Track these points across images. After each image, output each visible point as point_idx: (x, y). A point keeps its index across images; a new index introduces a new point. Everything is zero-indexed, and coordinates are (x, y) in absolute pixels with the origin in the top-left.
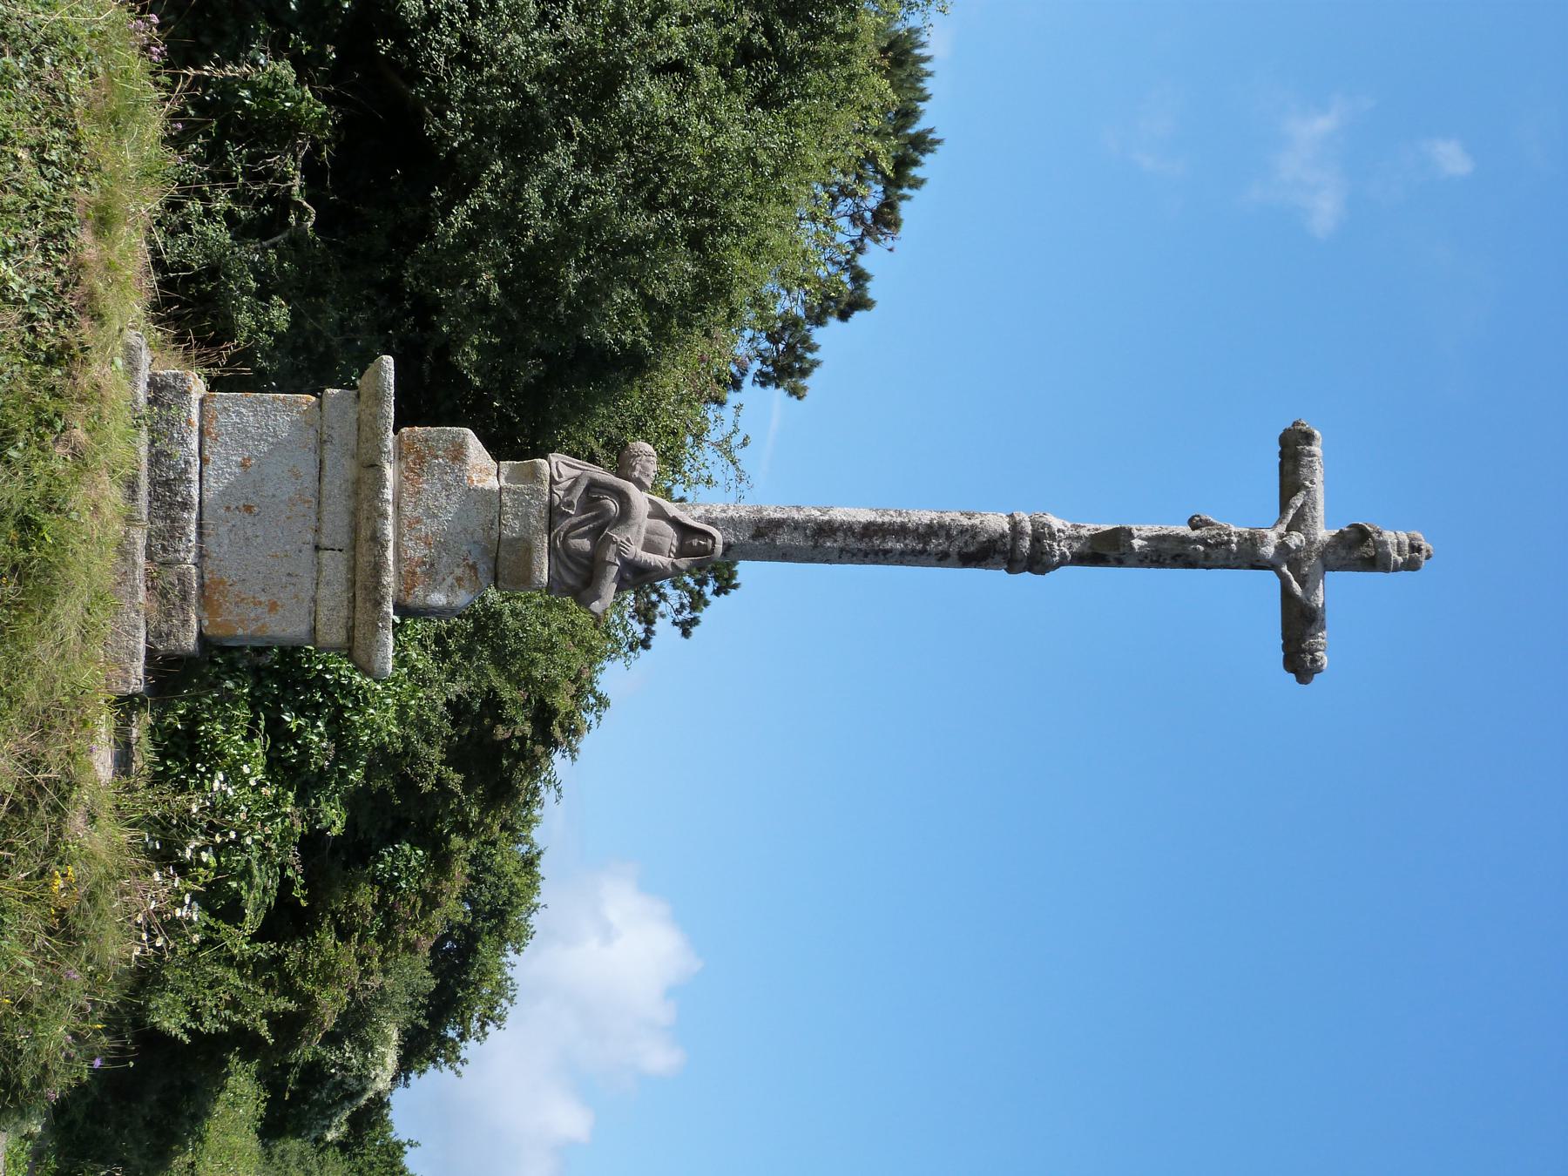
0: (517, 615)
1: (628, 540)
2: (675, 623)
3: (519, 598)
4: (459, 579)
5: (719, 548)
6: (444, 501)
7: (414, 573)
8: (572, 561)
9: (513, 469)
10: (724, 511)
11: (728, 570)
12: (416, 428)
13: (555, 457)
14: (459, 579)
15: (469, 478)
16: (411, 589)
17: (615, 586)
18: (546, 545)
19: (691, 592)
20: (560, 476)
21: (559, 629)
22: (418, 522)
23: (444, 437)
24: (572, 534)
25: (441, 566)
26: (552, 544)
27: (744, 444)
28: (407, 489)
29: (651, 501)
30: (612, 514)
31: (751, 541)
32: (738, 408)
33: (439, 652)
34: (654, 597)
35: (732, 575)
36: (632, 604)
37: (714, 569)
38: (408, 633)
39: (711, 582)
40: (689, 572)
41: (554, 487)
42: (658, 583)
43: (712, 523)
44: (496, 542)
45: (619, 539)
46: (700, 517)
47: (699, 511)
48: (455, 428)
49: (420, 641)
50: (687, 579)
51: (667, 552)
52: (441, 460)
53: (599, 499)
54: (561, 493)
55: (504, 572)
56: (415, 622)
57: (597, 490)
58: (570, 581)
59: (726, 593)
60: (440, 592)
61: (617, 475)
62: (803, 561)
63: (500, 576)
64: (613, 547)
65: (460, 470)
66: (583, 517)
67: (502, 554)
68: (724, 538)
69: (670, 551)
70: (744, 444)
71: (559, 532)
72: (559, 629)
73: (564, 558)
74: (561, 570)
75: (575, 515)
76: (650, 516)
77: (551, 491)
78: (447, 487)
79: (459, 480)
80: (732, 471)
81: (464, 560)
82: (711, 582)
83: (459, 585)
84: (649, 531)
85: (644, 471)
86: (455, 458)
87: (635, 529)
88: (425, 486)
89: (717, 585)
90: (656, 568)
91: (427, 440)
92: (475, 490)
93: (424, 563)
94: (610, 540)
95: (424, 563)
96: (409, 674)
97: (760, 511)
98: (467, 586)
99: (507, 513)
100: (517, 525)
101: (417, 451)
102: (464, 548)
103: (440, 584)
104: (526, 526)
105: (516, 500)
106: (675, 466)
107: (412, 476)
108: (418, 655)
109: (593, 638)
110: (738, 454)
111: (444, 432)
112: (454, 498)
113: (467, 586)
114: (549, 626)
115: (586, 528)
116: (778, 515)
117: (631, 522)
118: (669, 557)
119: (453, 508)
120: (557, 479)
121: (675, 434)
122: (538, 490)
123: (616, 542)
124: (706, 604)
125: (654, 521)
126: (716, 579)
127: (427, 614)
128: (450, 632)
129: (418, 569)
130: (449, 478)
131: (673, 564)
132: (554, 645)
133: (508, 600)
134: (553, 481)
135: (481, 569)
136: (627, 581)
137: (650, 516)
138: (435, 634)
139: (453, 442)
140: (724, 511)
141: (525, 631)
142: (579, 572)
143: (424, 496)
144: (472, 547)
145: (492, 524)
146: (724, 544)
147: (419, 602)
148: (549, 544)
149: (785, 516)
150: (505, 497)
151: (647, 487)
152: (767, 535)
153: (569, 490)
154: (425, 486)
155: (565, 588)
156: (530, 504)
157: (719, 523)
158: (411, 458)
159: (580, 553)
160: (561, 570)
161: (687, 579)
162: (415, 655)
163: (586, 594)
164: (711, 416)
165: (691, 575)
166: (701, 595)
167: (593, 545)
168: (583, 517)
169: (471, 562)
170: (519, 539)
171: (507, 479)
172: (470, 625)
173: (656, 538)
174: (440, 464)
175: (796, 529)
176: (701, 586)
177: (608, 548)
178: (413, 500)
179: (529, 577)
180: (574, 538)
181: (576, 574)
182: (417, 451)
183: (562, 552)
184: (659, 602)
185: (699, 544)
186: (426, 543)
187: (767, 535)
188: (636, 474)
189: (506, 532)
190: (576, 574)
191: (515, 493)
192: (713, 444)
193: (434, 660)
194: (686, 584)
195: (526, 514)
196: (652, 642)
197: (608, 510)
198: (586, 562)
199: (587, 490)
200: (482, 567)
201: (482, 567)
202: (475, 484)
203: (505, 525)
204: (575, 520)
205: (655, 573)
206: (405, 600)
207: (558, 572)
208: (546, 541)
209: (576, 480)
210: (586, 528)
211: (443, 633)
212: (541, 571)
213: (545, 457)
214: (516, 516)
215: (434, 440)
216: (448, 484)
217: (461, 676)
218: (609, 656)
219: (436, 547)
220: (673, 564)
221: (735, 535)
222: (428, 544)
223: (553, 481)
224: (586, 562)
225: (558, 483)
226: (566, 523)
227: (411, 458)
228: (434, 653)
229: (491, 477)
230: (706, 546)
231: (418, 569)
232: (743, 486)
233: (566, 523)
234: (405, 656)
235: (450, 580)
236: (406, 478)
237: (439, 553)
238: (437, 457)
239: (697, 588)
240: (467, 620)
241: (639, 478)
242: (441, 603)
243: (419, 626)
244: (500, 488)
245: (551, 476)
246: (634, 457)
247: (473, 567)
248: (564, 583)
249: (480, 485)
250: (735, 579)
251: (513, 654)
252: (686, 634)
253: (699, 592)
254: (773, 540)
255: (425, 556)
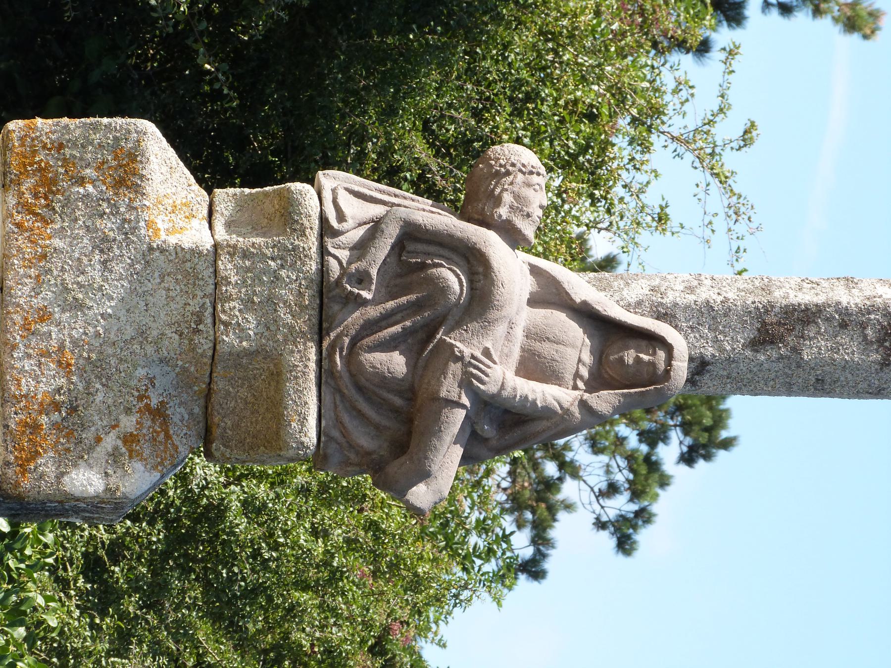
0: (259, 511)
1: (487, 353)
2: (600, 525)
3: (261, 477)
4: (129, 439)
5: (681, 369)
6: (97, 275)
7: (36, 427)
8: (369, 400)
9: (241, 205)
10: (691, 290)
11: (711, 408)
12: (39, 121)
13: (330, 179)
14: (129, 439)
15: (149, 224)
16: (28, 460)
17: (458, 452)
18: (312, 365)
19: (631, 458)
20: (341, 218)
21: (348, 541)
22: (42, 320)
23: (97, 137)
24: (368, 341)
25: (91, 411)
26: (325, 364)
27: (747, 137)
28: (19, 249)
29: (535, 271)
30: (453, 298)
31: (748, 353)
32: (732, 53)
33: (92, 593)
34: (551, 469)
35: (720, 419)
36: (505, 484)
37: (680, 408)
38: (28, 552)
39: (675, 435)
40: (625, 412)
41: (329, 243)
42: (561, 442)
43: (665, 315)
44: (208, 361)
45: (467, 352)
46: (639, 303)
47: (637, 291)
48: (119, 121)
49: (53, 570)
50: (623, 430)
51: (569, 377)
52: (90, 188)
53: (423, 266)
54: (344, 255)
55: (223, 423)
56: (41, 530)
57: (420, 247)
58: (364, 440)
59: (708, 457)
60: (90, 467)
61: (464, 214)
62: (858, 394)
63: (217, 432)
64: (455, 368)
65: (131, 208)
66: (391, 304)
67: (220, 385)
68: (691, 346)
69: (577, 375)
70: (747, 137)
71: (339, 337)
72: (348, 541)
73: (350, 391)
74: (346, 418)
75: (375, 302)
76: (534, 301)
77: (323, 251)
78: (103, 244)
79: (128, 229)
80: (717, 200)
81: (140, 398)
82: (675, 435)
83: (131, 451)
84: (533, 334)
85: (520, 206)
86: (120, 183)
87: (500, 329)
88: (57, 243)
89: (688, 441)
90: (547, 413)
91: (61, 146)
92: (162, 251)
93: (57, 406)
94: (451, 355)
95: (57, 406)
96: (30, 639)
97: (766, 289)
98: (147, 452)
99: (229, 299)
100: (251, 323)
101: (40, 169)
102: (141, 372)
103: (91, 449)
104: (269, 325)
105: (248, 270)
106: (596, 186)
107: (29, 221)
108: (48, 599)
109: (421, 558)
110: (730, 160)
111: (95, 128)
112: (118, 268)
113: (147, 452)
114: (326, 535)
115: (397, 329)
116: (806, 297)
117: (492, 315)
118: (575, 388)
119: (117, 289)
120: (334, 223)
121: (592, 117)
122: (295, 248)
123: (461, 359)
124: (664, 481)
125: (541, 314)
126: (686, 428)
127: (64, 513)
128: (116, 551)
129: (44, 420)
130: (108, 226)
131: (583, 404)
132: (336, 575)
133: (238, 480)
134: (326, 230)
135: (176, 419)
136: (485, 440)
137: (534, 301)
138: (85, 555)
139: (116, 147)
140: (691, 290)
141: (276, 547)
142: (385, 422)
143: (55, 264)
144: (156, 371)
145: (200, 321)
146: (691, 359)
147: (46, 488)
148: (319, 362)
149: (820, 299)
150: (226, 266)
151: (525, 239)
152: (782, 339)
153: (361, 248)
154: (57, 243)
155: (352, 456)
156: (277, 278)
157: (680, 315)
158: (28, 183)
159: (385, 381)
160: (346, 418)
161: (623, 430)
162: (40, 600)
163: (395, 468)
164: (667, 79)
165: (632, 422)
166: (652, 465)
167: (412, 365)
168: (391, 304)
169: (154, 402)
170: (257, 352)
171: (230, 225)
172: (158, 535)
173: (546, 349)
174: (87, 195)
175: (843, 325)
176: (653, 445)
177: (444, 373)
178: (33, 272)
179: (277, 433)
180: (371, 349)
181: (377, 427)
182: (40, 169)
183: (346, 376)
184: (561, 479)
185: (638, 360)
186: (59, 363)
187: (782, 339)
188: (503, 212)
189: (229, 339)
190: (377, 427)
191: (245, 255)
192: (673, 138)
193: (83, 610)
194: (620, 441)
195: (269, 299)
196: (548, 565)
197: (443, 290)
198: (398, 401)
199: (399, 247)
200: (177, 413)
201: (177, 413)
202: (163, 236)
203: (226, 324)
204: (373, 312)
205: (544, 424)
206: (17, 485)
207: (339, 422)
208: (313, 356)
209: (376, 227)
210: (397, 329)
211: (101, 552)
212: (303, 420)
213: (311, 181)
214: (248, 304)
215: (75, 145)
216: (105, 239)
217: (140, 643)
218: (456, 596)
219: (82, 371)
220: (583, 404)
221: (716, 340)
222: (64, 366)
223: (326, 230)
224: (398, 401)
225: (336, 233)
226: (356, 318)
227: (28, 183)
228: (80, 593)
229: (195, 223)
230: (652, 364)
231: (44, 420)
232: (741, 228)
233: (356, 318)
234: (22, 602)
235: (110, 441)
236: (19, 225)
237: (88, 383)
238: (81, 181)
239: (644, 448)
240: (151, 523)
241: (509, 222)
242: (91, 491)
243: (49, 538)
244: (216, 246)
245: (323, 219)
246: (498, 176)
247: (159, 413)
248: (351, 446)
249: (173, 240)
250: (725, 427)
251: (253, 592)
252: (625, 545)
253: (647, 459)
254: (796, 350)
255: (58, 390)
